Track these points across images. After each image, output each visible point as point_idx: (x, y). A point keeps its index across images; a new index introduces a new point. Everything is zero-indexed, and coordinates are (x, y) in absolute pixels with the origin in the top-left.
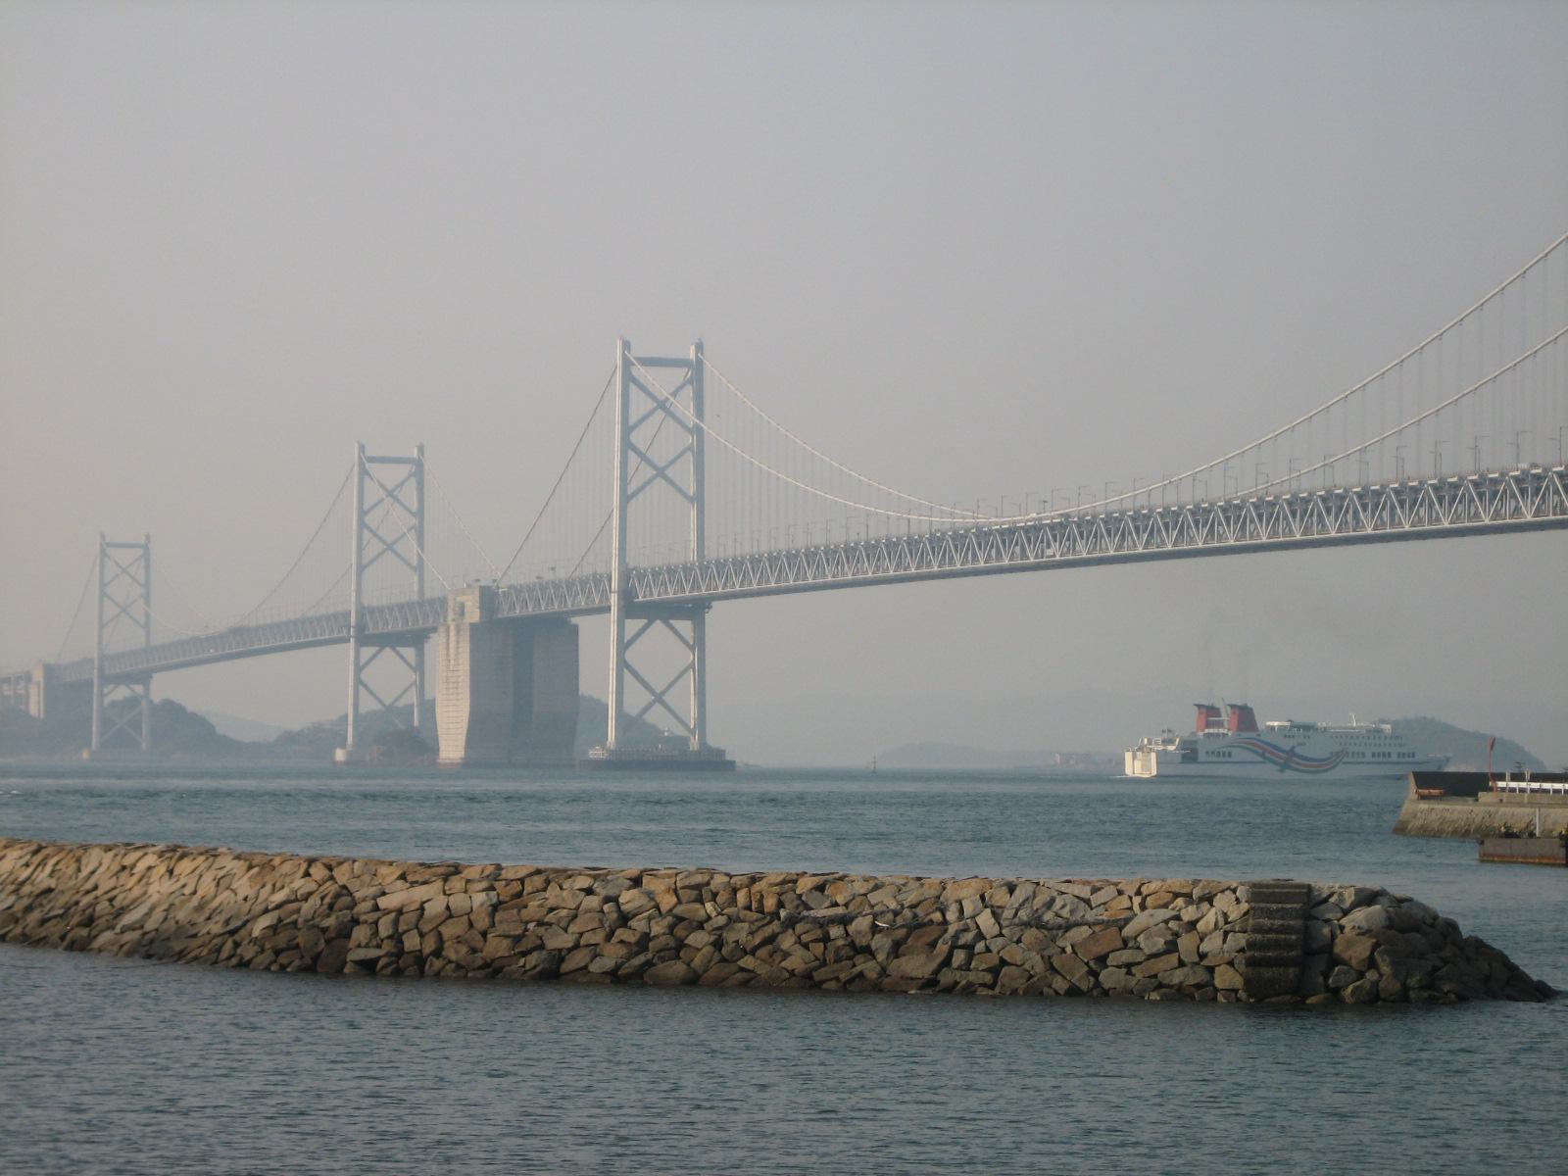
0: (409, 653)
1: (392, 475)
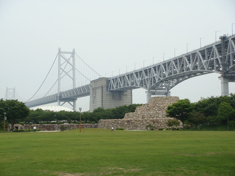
0: (72, 103)
1: (68, 56)
